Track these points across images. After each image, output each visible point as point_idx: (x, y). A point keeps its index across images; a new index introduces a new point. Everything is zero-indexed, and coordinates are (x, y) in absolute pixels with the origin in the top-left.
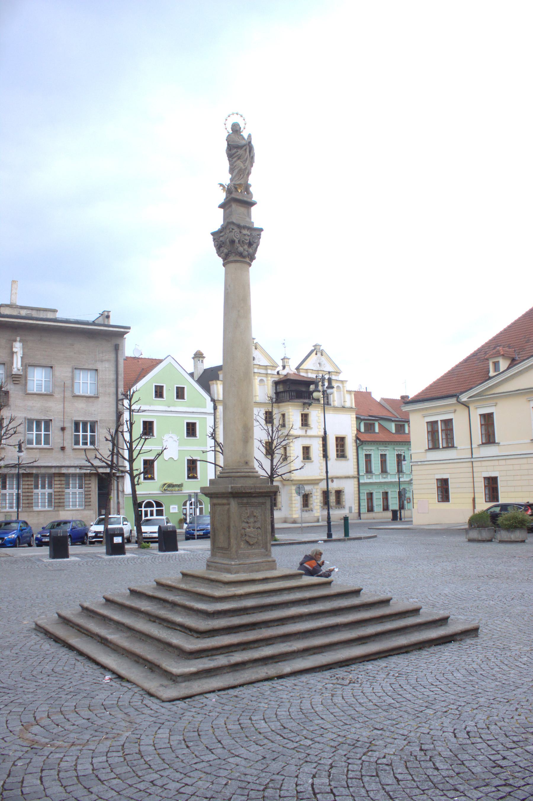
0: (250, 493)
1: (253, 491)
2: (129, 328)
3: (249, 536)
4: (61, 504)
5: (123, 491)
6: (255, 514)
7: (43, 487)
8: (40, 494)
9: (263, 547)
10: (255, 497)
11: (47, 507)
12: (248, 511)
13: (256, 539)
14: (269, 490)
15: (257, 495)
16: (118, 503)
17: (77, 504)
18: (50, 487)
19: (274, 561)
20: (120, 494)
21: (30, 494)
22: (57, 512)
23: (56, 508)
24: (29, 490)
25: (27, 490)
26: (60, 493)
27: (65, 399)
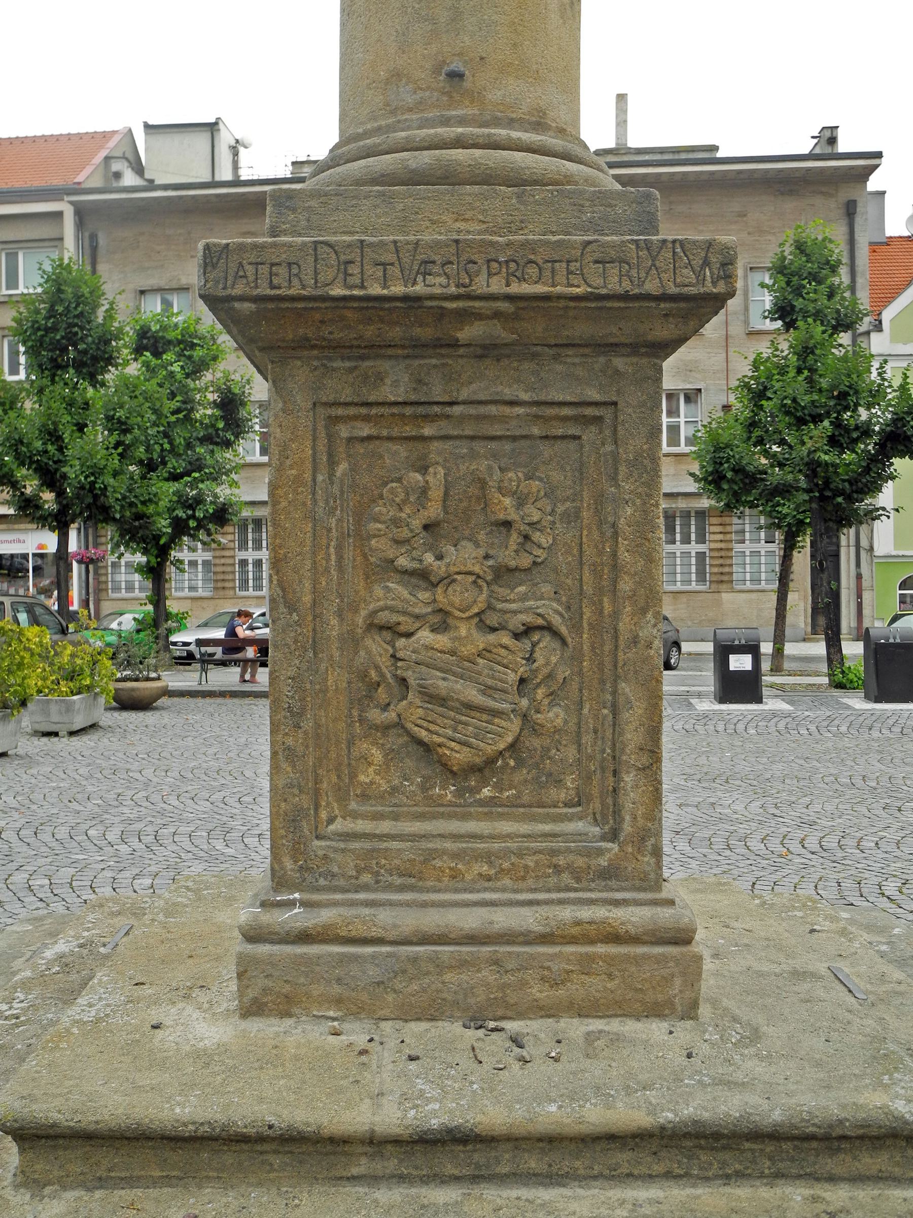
1: (435, 285)
2: (879, 155)
3: (432, 697)
4: (725, 578)
5: (871, 549)
7: (686, 540)
8: (678, 554)
11: (694, 583)
12: (436, 478)
13: (515, 725)
14: (614, 284)
16: (859, 577)
17: (763, 577)
18: (701, 539)
19: (682, 937)
20: (863, 555)
22: (716, 595)
23: (714, 586)
26: (723, 553)
27: (730, 340)
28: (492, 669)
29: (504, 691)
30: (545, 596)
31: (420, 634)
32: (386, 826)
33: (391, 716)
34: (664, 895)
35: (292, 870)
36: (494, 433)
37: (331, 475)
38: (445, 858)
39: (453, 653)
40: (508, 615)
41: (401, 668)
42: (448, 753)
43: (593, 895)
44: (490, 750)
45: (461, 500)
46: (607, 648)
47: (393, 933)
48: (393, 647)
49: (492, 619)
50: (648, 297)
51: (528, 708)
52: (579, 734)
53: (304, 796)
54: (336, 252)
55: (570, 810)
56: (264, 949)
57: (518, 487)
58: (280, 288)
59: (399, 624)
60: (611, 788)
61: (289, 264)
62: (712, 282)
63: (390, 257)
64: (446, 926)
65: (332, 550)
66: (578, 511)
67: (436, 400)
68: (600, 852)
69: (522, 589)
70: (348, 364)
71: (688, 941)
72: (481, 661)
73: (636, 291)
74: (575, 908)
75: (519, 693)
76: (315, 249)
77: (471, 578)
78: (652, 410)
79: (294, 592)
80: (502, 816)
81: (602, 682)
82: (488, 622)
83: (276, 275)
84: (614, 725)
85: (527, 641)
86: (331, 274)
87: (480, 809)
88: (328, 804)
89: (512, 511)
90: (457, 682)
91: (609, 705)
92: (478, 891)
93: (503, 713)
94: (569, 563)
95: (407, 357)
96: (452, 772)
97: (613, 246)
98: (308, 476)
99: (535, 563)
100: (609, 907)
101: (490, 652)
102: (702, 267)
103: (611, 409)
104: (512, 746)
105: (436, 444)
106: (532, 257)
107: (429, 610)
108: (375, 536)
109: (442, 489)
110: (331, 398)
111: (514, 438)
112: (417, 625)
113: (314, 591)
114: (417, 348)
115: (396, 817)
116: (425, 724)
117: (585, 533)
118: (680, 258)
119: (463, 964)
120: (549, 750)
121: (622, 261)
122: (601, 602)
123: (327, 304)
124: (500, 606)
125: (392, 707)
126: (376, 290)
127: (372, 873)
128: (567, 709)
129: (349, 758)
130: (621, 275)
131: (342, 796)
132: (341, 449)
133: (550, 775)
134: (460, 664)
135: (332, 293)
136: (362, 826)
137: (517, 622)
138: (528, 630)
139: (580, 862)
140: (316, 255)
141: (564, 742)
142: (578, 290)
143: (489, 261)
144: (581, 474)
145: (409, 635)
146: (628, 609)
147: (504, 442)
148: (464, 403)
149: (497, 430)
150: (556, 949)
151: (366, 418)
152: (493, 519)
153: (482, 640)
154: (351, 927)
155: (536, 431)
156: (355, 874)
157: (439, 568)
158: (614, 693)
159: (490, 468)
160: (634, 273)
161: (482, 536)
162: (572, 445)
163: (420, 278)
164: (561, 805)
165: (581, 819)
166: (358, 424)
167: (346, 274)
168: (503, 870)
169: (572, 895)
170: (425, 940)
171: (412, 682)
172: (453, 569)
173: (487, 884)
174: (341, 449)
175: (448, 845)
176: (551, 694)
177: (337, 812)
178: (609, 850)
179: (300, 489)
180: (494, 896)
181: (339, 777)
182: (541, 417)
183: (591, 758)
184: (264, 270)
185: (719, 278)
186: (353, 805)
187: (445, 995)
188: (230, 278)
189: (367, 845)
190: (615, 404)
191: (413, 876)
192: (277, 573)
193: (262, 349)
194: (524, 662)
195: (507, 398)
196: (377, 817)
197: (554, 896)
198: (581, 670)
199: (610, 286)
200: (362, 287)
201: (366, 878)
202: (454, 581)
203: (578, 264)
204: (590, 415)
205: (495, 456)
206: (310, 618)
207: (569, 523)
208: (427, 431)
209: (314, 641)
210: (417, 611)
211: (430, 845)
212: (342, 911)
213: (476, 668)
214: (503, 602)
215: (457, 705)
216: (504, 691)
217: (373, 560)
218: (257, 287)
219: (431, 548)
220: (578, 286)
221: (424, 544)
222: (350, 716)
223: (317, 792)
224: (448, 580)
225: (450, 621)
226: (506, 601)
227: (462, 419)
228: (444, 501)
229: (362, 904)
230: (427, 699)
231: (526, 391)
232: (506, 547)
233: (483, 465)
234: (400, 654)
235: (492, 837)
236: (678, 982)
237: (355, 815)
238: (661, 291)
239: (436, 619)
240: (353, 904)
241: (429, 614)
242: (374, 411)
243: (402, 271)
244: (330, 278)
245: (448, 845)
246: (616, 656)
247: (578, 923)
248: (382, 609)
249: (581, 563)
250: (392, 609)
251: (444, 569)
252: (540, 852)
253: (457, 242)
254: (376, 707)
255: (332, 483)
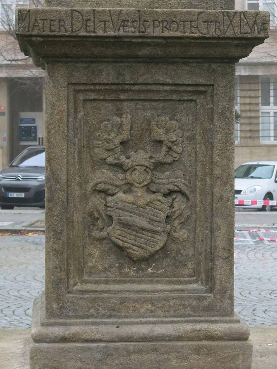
0: (117, 41)
1: (129, 31)
3: (126, 225)
6: (160, 134)
9: (196, 273)
10: (152, 60)
12: (127, 119)
14: (212, 32)
15: (159, 52)
19: (242, 337)
21: (253, 114)
24: (253, 107)
25: (247, 108)
28: (153, 211)
29: (160, 222)
30: (179, 176)
31: (118, 195)
32: (101, 287)
33: (104, 234)
34: (235, 318)
35: (56, 308)
36: (154, 98)
37: (76, 118)
38: (131, 302)
39: (134, 204)
40: (161, 186)
41: (109, 211)
42: (132, 251)
43: (201, 319)
44: (152, 250)
45: (138, 130)
46: (208, 201)
47: (106, 336)
48: (105, 201)
49: (154, 188)
50: (228, 38)
51: (171, 230)
52: (194, 242)
53: (62, 273)
54: (82, 15)
55: (190, 279)
56: (45, 345)
57: (166, 124)
58: (55, 31)
59: (108, 189)
60: (210, 268)
61: (60, 21)
62: (258, 32)
63: (108, 18)
64: (132, 333)
65: (76, 154)
66: (194, 135)
67: (127, 83)
68: (205, 298)
69: (168, 173)
70: (84, 65)
71: (246, 339)
72: (148, 207)
73: (223, 36)
74: (192, 324)
75: (166, 223)
76: (72, 14)
77: (144, 168)
78: (230, 88)
79: (58, 175)
80: (158, 282)
81: (206, 217)
82: (151, 189)
83: (53, 25)
84: (211, 238)
85: (170, 198)
86: (79, 25)
87: (148, 279)
88: (73, 277)
89: (163, 136)
90: (136, 218)
91: (209, 228)
92: (147, 317)
93: (159, 232)
94: (190, 161)
95: (114, 62)
96: (133, 261)
97: (211, 14)
98: (65, 119)
99: (174, 160)
100: (209, 324)
101: (152, 203)
102: (254, 25)
103: (211, 88)
104: (162, 248)
105: (126, 103)
106: (174, 19)
107: (123, 183)
108: (96, 147)
109: (130, 125)
110: (76, 81)
111: (164, 101)
112: (117, 190)
113: (68, 174)
114: (118, 59)
115: (106, 282)
116: (121, 238)
117: (198, 146)
118: (243, 20)
119: (139, 351)
120: (180, 250)
121: (216, 22)
122: (205, 179)
123: (77, 39)
124: (157, 181)
125: (105, 230)
126: (100, 33)
127: (95, 309)
128: (189, 230)
129: (83, 255)
130: (216, 28)
131: (80, 273)
132: (80, 105)
133: (181, 262)
134: (138, 209)
135: (80, 34)
136: (89, 287)
137: (165, 189)
138: (169, 194)
139: (195, 303)
140: (72, 16)
141: (188, 247)
142: (196, 35)
143: (154, 21)
144: (196, 118)
145: (113, 195)
146: (219, 183)
147: (159, 102)
148: (141, 84)
149: (156, 97)
150: (185, 343)
151: (93, 91)
152: (154, 139)
153: (149, 197)
154: (86, 334)
155: (175, 97)
156: (87, 310)
157: (128, 163)
158: (211, 223)
159: (153, 115)
160: (222, 27)
161: (148, 147)
162: (192, 104)
163: (121, 28)
164: (186, 276)
165: (196, 283)
166: (90, 93)
167: (87, 26)
168: (158, 307)
169: (191, 318)
170: (122, 339)
171: (115, 218)
172: (134, 164)
173: (150, 314)
174: (80, 105)
175: (132, 295)
176: (182, 223)
177: (77, 281)
178: (209, 297)
179: (61, 125)
180: (155, 319)
181: (79, 263)
182: (178, 91)
183: (200, 254)
184: (47, 23)
185: (261, 30)
186: (85, 277)
187: (131, 366)
188: (31, 26)
189: (93, 296)
190: (213, 85)
191: (113, 312)
192: (50, 165)
193: (42, 58)
194: (169, 208)
195: (161, 82)
196: (97, 282)
197: (183, 319)
198: (196, 212)
199: (210, 33)
200: (94, 32)
201: (93, 311)
202: (135, 169)
203: (196, 23)
204: (199, 91)
205: (155, 109)
206: (66, 187)
207: (190, 141)
208: (122, 97)
209: (67, 198)
210: (117, 183)
211: (123, 296)
212: (83, 327)
213: (145, 211)
214: (159, 179)
215: (136, 228)
216: (160, 222)
217: (95, 159)
218: (44, 31)
219: (123, 153)
220: (196, 33)
221: (121, 151)
222: (84, 234)
223: (68, 271)
224: (132, 169)
225: (133, 188)
226: (160, 179)
227: (139, 91)
228: (130, 131)
229: (91, 324)
230: (122, 225)
231: (170, 79)
232: (160, 153)
233: (148, 114)
234: (108, 204)
235: (153, 292)
236: (241, 358)
237: (86, 282)
238: (234, 36)
239: (126, 188)
240: (86, 324)
241: (123, 185)
242: (96, 88)
243: (113, 25)
244: (79, 27)
245: (132, 295)
246: (212, 205)
247: (194, 331)
248: (100, 183)
249: (196, 161)
250: (105, 183)
251: (130, 164)
252: (176, 298)
253: (139, 11)
254: (97, 230)
255: (76, 122)
